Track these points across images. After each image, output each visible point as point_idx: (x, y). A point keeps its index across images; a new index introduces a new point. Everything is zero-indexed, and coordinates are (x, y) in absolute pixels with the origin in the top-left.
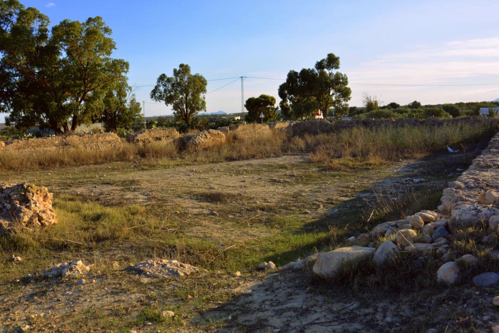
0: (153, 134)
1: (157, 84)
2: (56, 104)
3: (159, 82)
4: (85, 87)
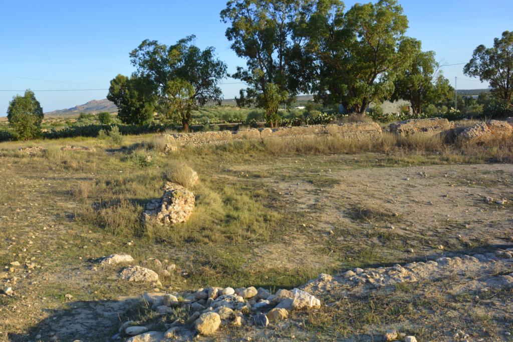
0: (419, 124)
1: (472, 58)
2: (347, 86)
3: (475, 54)
4: (375, 69)
